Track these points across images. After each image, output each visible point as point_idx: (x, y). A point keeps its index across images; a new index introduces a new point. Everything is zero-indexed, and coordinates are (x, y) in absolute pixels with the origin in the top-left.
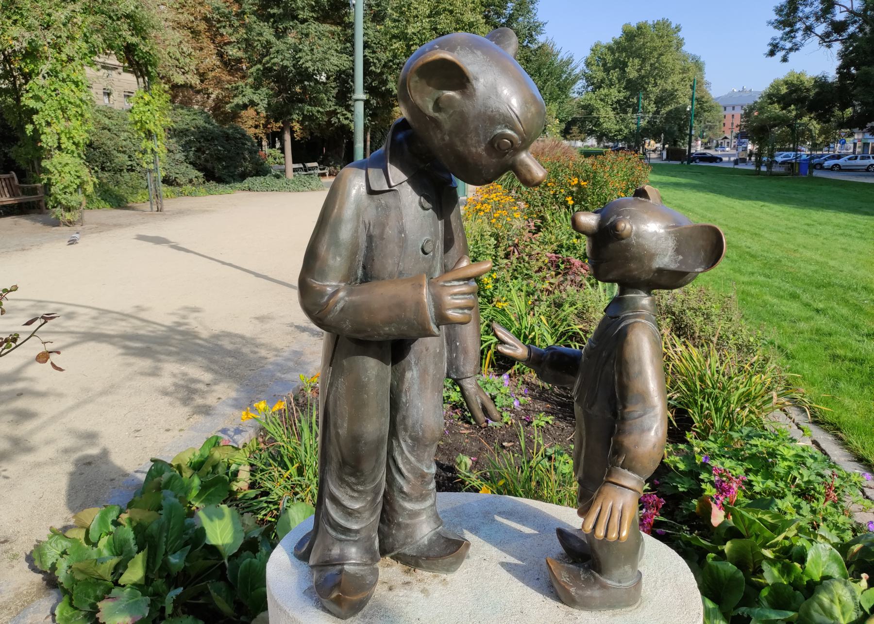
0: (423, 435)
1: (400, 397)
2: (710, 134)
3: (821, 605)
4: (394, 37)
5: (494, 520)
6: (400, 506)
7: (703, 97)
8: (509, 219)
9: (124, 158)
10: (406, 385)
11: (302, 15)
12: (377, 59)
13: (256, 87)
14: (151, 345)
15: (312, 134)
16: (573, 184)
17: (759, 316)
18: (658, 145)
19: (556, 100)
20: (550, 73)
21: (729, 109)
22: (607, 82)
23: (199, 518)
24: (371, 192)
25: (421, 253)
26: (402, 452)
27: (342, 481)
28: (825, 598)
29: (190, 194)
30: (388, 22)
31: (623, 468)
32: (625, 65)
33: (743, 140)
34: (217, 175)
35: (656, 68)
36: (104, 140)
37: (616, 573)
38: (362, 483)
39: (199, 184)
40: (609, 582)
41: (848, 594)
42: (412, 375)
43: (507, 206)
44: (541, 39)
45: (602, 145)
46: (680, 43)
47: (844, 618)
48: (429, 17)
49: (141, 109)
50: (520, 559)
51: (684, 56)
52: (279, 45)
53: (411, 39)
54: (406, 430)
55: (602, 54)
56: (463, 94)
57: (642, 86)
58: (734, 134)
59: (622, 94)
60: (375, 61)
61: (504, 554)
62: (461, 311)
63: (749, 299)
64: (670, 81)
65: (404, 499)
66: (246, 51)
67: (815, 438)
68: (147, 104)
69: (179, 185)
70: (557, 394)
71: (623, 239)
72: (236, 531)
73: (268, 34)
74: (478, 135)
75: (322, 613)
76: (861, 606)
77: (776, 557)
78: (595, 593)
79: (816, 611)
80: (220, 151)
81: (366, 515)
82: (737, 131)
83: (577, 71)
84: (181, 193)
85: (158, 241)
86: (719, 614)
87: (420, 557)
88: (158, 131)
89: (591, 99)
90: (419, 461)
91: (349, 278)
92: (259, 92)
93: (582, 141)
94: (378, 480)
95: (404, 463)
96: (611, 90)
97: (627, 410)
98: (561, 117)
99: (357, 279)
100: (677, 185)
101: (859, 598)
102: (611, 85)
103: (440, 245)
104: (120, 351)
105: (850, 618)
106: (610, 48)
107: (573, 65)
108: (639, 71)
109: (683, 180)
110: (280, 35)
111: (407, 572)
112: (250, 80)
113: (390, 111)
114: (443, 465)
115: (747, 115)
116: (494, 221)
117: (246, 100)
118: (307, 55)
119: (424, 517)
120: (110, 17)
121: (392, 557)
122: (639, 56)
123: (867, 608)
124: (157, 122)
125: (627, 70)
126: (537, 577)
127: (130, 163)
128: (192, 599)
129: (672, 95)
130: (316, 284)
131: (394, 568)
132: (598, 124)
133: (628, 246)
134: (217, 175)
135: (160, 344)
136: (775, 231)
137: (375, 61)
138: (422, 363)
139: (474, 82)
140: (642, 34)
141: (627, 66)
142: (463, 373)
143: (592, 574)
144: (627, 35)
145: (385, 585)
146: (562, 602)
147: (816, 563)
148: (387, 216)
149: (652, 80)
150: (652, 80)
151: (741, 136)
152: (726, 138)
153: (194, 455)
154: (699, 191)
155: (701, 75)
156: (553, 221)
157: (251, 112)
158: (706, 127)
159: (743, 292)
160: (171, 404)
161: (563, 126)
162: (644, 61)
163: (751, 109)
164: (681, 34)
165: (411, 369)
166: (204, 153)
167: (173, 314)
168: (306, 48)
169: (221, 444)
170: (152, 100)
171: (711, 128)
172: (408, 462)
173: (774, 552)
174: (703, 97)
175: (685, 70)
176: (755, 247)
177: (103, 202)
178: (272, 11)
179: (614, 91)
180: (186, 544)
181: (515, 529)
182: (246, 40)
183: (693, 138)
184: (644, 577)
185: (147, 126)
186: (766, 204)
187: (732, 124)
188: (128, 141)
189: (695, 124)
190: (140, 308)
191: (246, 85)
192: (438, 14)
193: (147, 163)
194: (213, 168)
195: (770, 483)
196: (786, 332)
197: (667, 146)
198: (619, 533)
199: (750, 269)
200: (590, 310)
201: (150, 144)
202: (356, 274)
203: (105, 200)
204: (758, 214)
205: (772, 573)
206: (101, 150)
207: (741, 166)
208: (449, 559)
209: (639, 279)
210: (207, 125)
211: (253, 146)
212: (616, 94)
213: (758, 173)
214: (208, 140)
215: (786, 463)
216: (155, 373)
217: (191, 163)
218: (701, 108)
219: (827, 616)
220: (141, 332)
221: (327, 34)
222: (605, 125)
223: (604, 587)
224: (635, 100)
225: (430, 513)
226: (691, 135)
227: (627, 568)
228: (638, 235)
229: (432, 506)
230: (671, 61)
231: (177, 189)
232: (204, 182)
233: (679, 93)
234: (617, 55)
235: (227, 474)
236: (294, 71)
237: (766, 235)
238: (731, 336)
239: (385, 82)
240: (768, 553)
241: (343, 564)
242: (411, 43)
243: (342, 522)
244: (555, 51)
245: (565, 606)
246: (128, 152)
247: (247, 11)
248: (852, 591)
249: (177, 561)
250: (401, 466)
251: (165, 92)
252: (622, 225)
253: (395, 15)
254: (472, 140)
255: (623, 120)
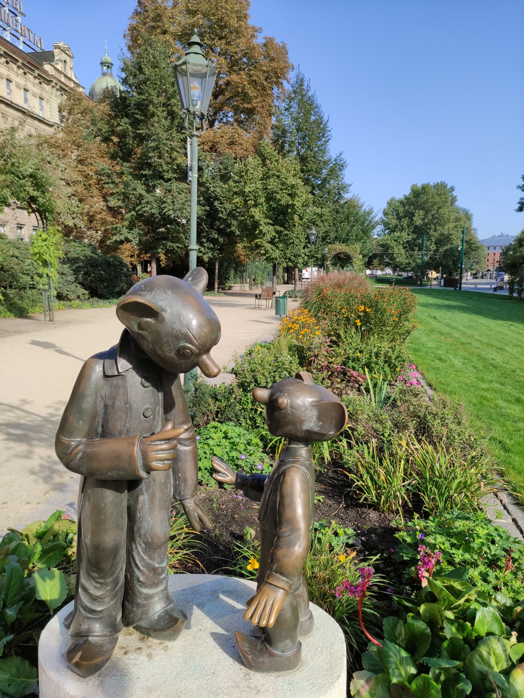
0: (152, 541)
1: (135, 513)
2: (477, 267)
3: (481, 656)
4: (235, 193)
5: (218, 597)
6: (138, 591)
7: (471, 240)
8: (312, 336)
9: (27, 279)
10: (140, 506)
11: (167, 176)
12: (224, 208)
13: (131, 227)
14: (27, 432)
15: (174, 262)
16: (360, 310)
17: (490, 417)
18: (438, 275)
19: (360, 240)
20: (356, 221)
21: (492, 249)
22: (399, 227)
23: (34, 578)
24: (106, 376)
25: (143, 417)
26: (139, 553)
27: (90, 576)
28: (483, 650)
29: (77, 307)
30: (231, 183)
31: (276, 573)
32: (413, 215)
33: (501, 273)
34: (99, 293)
35: (436, 218)
36: (12, 265)
37: (280, 645)
38: (103, 578)
39: (86, 299)
40: (275, 652)
41: (501, 648)
42: (144, 498)
43: (311, 325)
44: (347, 196)
45: (396, 274)
46: (454, 200)
47: (498, 667)
48: (261, 180)
49: (40, 244)
50: (227, 632)
51: (457, 209)
52: (148, 197)
53: (247, 196)
54: (140, 537)
55: (395, 207)
56: (157, 320)
57: (426, 231)
58: (495, 268)
59: (410, 237)
60: (223, 210)
61: (216, 626)
62: (161, 462)
63: (485, 402)
64: (446, 227)
65: (141, 586)
66: (123, 201)
67: (514, 516)
68: (45, 240)
69: (69, 300)
70: (330, 477)
71: (282, 409)
72: (62, 590)
73: (141, 189)
74: (170, 346)
75: (70, 672)
76: (510, 657)
77: (455, 617)
78: (265, 659)
79: (477, 661)
80: (102, 274)
81: (107, 600)
82: (497, 265)
83: (377, 219)
84: (71, 306)
85: (47, 345)
86: (410, 661)
87: (150, 629)
88: (52, 261)
89: (387, 239)
90: (151, 559)
91: (91, 434)
92: (133, 232)
93: (381, 270)
94: (115, 575)
95: (140, 561)
96: (403, 234)
97: (281, 531)
98: (364, 253)
99: (97, 434)
100: (449, 307)
101: (509, 651)
102: (402, 230)
103: (160, 409)
104: (5, 437)
105: (502, 667)
106: (401, 202)
107: (373, 215)
108: (423, 219)
109: (454, 303)
110: (150, 190)
111: (142, 640)
112: (126, 223)
113: (234, 247)
114: (235, 534)
115: (504, 254)
116: (301, 337)
117: (122, 238)
118: (170, 205)
119: (156, 599)
120: (18, 177)
121: (134, 628)
122: (423, 209)
123: (515, 659)
124: (52, 254)
125: (414, 219)
126: (234, 644)
127: (32, 283)
128: (24, 642)
129: (448, 238)
130: (65, 439)
131: (133, 636)
132: (392, 258)
133: (286, 414)
134: (99, 293)
135: (35, 432)
136: (516, 346)
137: (223, 210)
138: (151, 490)
139: (163, 313)
140: (426, 192)
141: (414, 216)
142: (183, 496)
143: (265, 645)
144: (414, 193)
145: (123, 650)
146: (245, 666)
147: (482, 622)
148: (117, 393)
149: (433, 227)
150: (433, 227)
151: (500, 269)
152: (489, 270)
153: (40, 526)
154: (464, 312)
155: (470, 223)
156: (345, 338)
157: (127, 246)
158: (475, 262)
159: (482, 397)
160: (36, 482)
161: (366, 259)
162: (427, 212)
163: (508, 249)
164: (455, 193)
165: (143, 494)
166: (90, 276)
167: (49, 407)
168: (169, 201)
169: (62, 518)
170: (49, 238)
171: (478, 263)
172: (143, 560)
173: (454, 613)
174: (471, 240)
175: (457, 220)
176: (497, 358)
177: (9, 313)
178: (144, 173)
179: (404, 234)
180: (21, 600)
181: (231, 606)
182: (124, 193)
183: (464, 270)
184: (303, 647)
185: (44, 257)
186: (514, 323)
187: (494, 260)
188: (31, 266)
189: (465, 260)
190: (25, 402)
191: (123, 226)
192: (268, 177)
193: (43, 284)
194: (97, 287)
195: (467, 556)
196: (508, 430)
197: (444, 276)
198: (268, 621)
199: (490, 378)
200: (358, 412)
201: (46, 271)
202: (96, 430)
203: (10, 311)
204: (506, 332)
205: (451, 629)
206: (10, 273)
207: (499, 293)
208: (168, 632)
209: (296, 436)
210: (93, 255)
211: (129, 271)
212: (406, 236)
213: (511, 298)
214: (94, 266)
215: (480, 540)
216: (28, 456)
217: (79, 283)
218: (470, 248)
219: (485, 664)
220: (23, 421)
221: (185, 191)
222: (398, 259)
223: (272, 655)
224: (420, 241)
225: (161, 596)
226: (462, 269)
227: (288, 642)
228: (292, 407)
229: (163, 590)
230: (447, 213)
231: (68, 303)
232: (89, 298)
233: (453, 236)
234: (407, 207)
235: (66, 542)
236: (159, 217)
237: (509, 350)
238: (457, 437)
239: (229, 226)
240: (450, 615)
241: (88, 636)
242: (248, 199)
243: (89, 605)
244: (360, 205)
245: (246, 669)
246: (31, 274)
247: (125, 172)
248: (504, 646)
249: (12, 613)
250: (138, 562)
251: (59, 231)
252: (281, 400)
253: (237, 178)
254: (166, 348)
255: (411, 256)
